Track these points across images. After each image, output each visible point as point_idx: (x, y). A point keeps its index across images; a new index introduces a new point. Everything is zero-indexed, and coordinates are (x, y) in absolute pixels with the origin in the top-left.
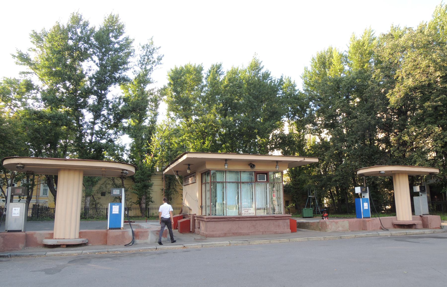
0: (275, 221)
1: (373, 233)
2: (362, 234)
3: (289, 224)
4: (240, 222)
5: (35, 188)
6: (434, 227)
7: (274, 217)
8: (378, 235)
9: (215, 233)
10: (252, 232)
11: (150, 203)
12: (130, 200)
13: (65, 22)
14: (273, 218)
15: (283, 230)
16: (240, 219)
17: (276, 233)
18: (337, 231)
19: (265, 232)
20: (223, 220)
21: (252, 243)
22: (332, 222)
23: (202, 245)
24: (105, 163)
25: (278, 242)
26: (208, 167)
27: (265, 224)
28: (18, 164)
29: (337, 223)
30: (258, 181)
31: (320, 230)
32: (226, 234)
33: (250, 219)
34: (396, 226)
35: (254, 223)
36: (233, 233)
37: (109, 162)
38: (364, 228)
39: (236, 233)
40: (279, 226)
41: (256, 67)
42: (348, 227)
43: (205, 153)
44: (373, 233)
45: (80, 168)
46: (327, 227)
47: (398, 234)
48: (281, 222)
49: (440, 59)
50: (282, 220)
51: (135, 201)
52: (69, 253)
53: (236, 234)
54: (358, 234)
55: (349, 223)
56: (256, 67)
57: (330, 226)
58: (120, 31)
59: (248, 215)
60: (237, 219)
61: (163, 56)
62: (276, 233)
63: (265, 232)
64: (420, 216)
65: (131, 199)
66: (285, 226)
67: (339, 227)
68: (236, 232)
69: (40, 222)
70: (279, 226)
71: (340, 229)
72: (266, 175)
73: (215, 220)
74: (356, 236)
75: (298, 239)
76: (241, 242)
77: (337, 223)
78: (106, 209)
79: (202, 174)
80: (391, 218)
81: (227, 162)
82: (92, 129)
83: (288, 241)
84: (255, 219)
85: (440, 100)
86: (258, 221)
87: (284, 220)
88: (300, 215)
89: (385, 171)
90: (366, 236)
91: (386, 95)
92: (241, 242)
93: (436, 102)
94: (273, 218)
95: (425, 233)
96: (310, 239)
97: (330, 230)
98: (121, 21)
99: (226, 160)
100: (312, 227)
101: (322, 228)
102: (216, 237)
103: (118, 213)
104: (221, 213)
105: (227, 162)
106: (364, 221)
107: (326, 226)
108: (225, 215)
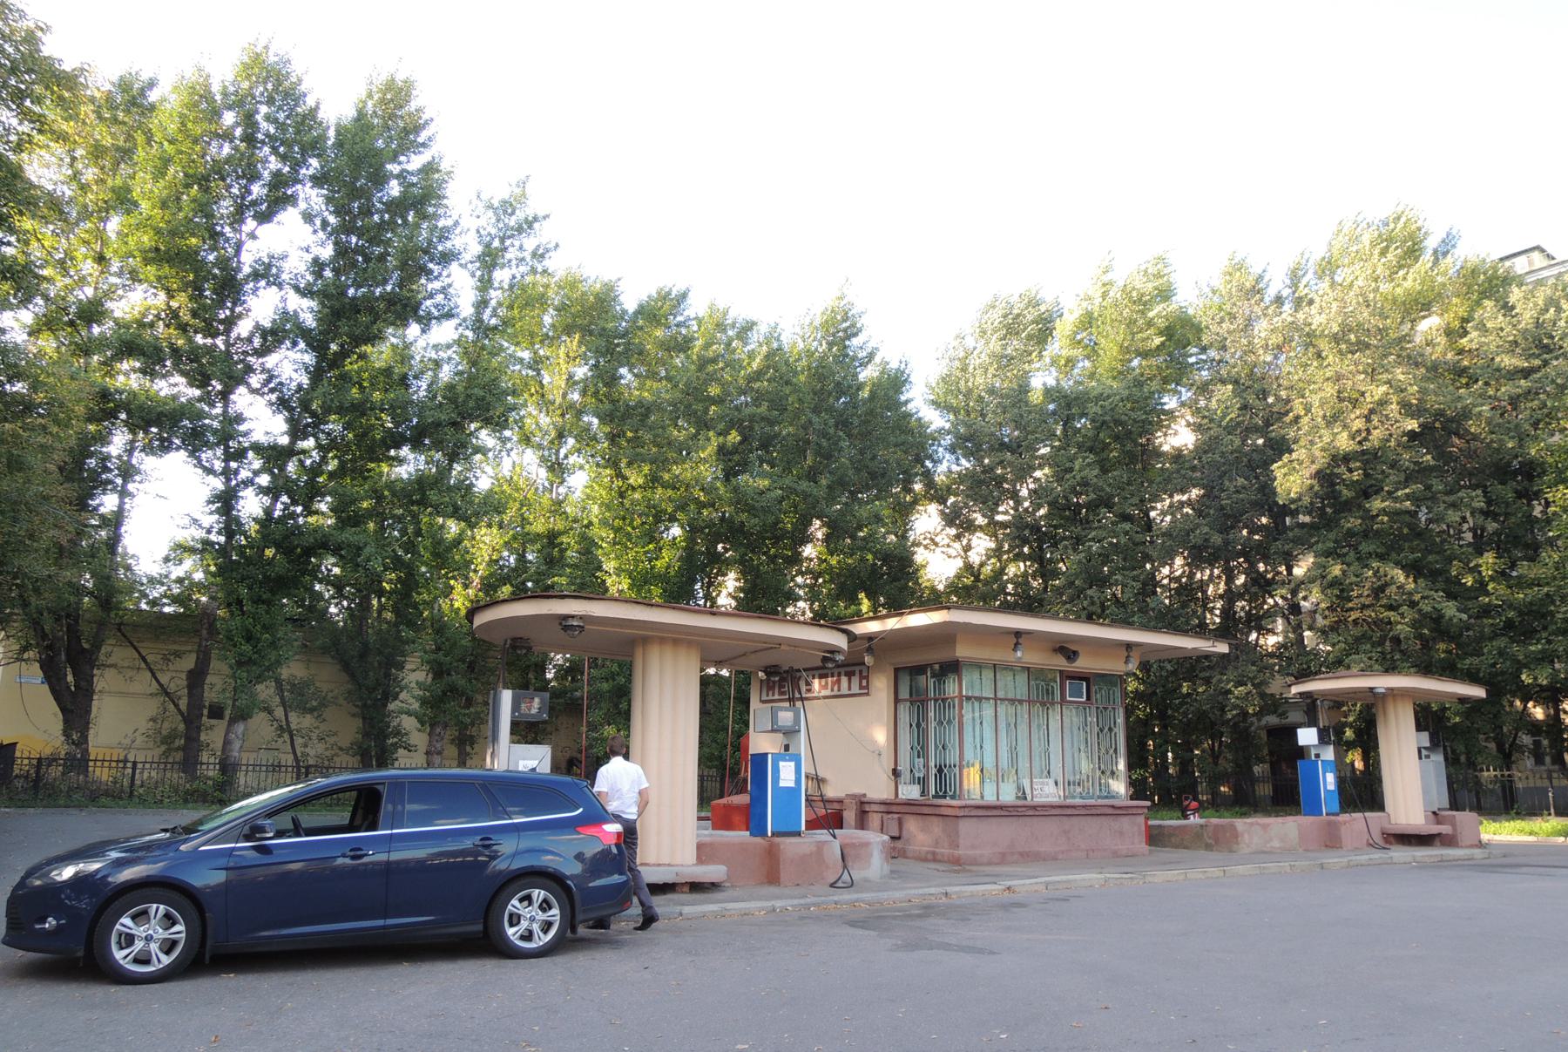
2: (1333, 859)
5: (787, 704)
6: (1469, 843)
7: (1113, 807)
9: (978, 852)
11: (401, 752)
12: (332, 740)
13: (223, 74)
14: (1110, 811)
16: (1023, 810)
17: (1116, 854)
21: (1150, 879)
22: (1252, 824)
23: (1047, 884)
24: (805, 627)
25: (1201, 876)
27: (1092, 825)
28: (573, 617)
29: (1265, 827)
31: (1208, 847)
32: (1003, 855)
34: (1392, 839)
36: (1021, 854)
37: (714, 614)
38: (1331, 840)
40: (1121, 833)
41: (841, 329)
45: (694, 635)
46: (1237, 837)
47: (1427, 859)
48: (1125, 822)
49: (1416, 388)
51: (345, 743)
52: (740, 909)
56: (841, 329)
57: (1246, 836)
58: (409, 134)
60: (1031, 813)
61: (557, 246)
62: (1116, 854)
64: (1434, 813)
65: (335, 734)
66: (1133, 829)
67: (1271, 840)
69: (72, 811)
70: (1121, 833)
71: (1276, 844)
73: (980, 812)
78: (129, 765)
79: (897, 671)
85: (1408, 497)
89: (1388, 689)
91: (1273, 468)
93: (1396, 499)
94: (1110, 811)
98: (423, 100)
99: (1018, 634)
100: (1173, 840)
101: (1220, 842)
103: (792, 784)
106: (1329, 823)
107: (1235, 835)
108: (1029, 798)
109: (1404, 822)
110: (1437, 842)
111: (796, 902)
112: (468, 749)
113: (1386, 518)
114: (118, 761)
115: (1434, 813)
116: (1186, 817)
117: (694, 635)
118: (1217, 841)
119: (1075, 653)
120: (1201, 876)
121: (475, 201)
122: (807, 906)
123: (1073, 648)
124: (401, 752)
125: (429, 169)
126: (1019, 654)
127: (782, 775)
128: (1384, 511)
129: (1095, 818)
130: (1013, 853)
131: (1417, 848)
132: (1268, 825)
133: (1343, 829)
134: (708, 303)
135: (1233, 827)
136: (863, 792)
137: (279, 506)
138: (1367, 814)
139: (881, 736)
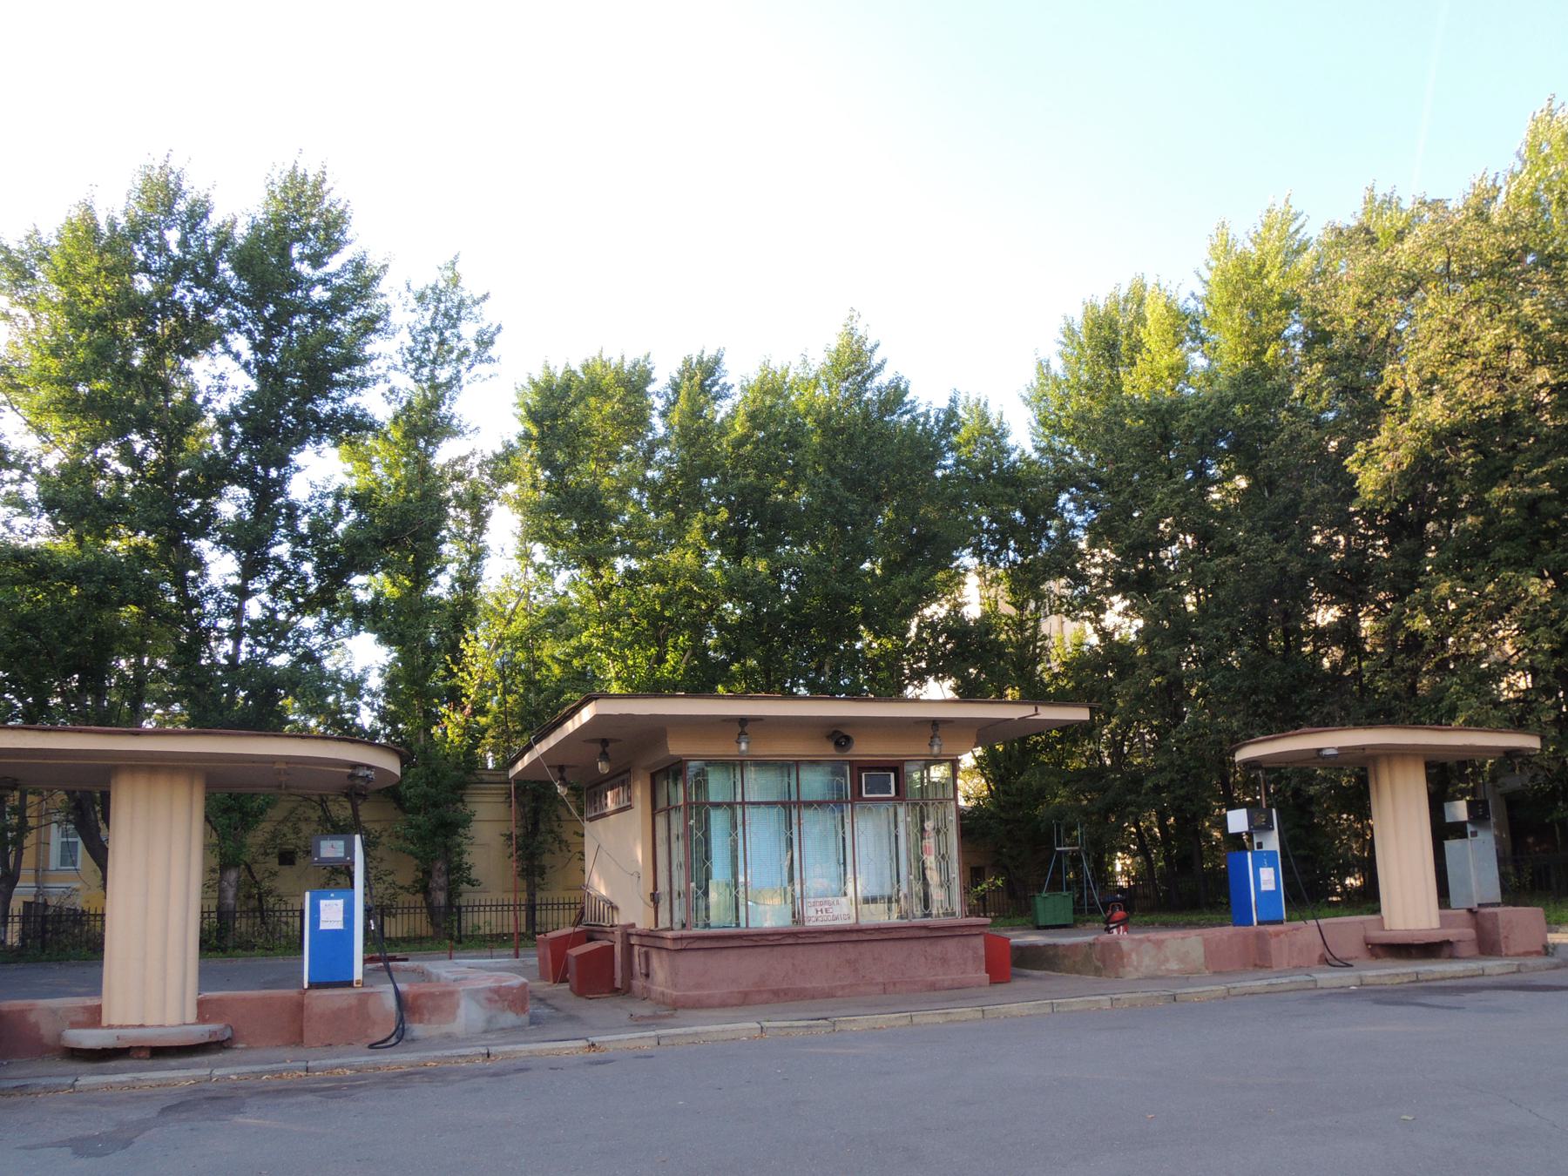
0: (927, 942)
1: (1293, 978)
3: (982, 952)
4: (800, 948)
8: (1311, 986)
10: (843, 988)
11: (464, 886)
12: (389, 879)
14: (923, 933)
17: (933, 987)
18: (1160, 973)
19: (894, 984)
21: (843, 1026)
22: (1141, 941)
23: (659, 1038)
25: (940, 1020)
27: (893, 953)
29: (1159, 944)
30: (864, 795)
31: (1098, 972)
32: (746, 994)
34: (1378, 950)
35: (851, 952)
36: (776, 993)
38: (1260, 960)
39: (786, 992)
40: (944, 961)
42: (1202, 960)
44: (1293, 978)
45: (188, 761)
46: (1122, 958)
47: (1387, 980)
48: (951, 947)
50: (956, 939)
52: (160, 1079)
54: (1238, 985)
55: (1206, 943)
56: (765, 367)
57: (1134, 956)
58: (331, 233)
59: (828, 923)
62: (933, 987)
63: (894, 984)
64: (1470, 910)
65: (392, 873)
67: (1167, 960)
68: (785, 986)
71: (1174, 965)
72: (892, 775)
73: (707, 944)
75: (1015, 1008)
77: (1159, 944)
80: (1362, 923)
82: (237, 613)
83: (979, 1015)
84: (854, 937)
85: (1549, 475)
86: (866, 944)
87: (962, 939)
89: (1339, 749)
90: (1292, 986)
91: (1346, 463)
93: (1533, 483)
94: (923, 933)
95: (1487, 972)
96: (1059, 1005)
97: (1136, 969)
98: (338, 193)
99: (743, 721)
101: (1104, 963)
103: (339, 926)
104: (729, 918)
108: (743, 924)
109: (1402, 927)
110: (1446, 950)
111: (245, 1069)
112: (537, 879)
113: (1511, 510)
114: (415, 908)
115: (1470, 910)
116: (1108, 930)
117: (188, 761)
118: (1104, 962)
119: (848, 739)
120: (940, 1020)
121: (405, 294)
122: (259, 1075)
123: (847, 732)
124: (464, 886)
125: (358, 267)
126: (743, 746)
127: (323, 917)
128: (1505, 501)
129: (899, 944)
130: (760, 992)
131: (1419, 962)
132: (1163, 941)
133: (1273, 941)
134: (542, 363)
135: (1115, 945)
136: (632, 921)
137: (243, 647)
138: (1321, 922)
139: (639, 853)
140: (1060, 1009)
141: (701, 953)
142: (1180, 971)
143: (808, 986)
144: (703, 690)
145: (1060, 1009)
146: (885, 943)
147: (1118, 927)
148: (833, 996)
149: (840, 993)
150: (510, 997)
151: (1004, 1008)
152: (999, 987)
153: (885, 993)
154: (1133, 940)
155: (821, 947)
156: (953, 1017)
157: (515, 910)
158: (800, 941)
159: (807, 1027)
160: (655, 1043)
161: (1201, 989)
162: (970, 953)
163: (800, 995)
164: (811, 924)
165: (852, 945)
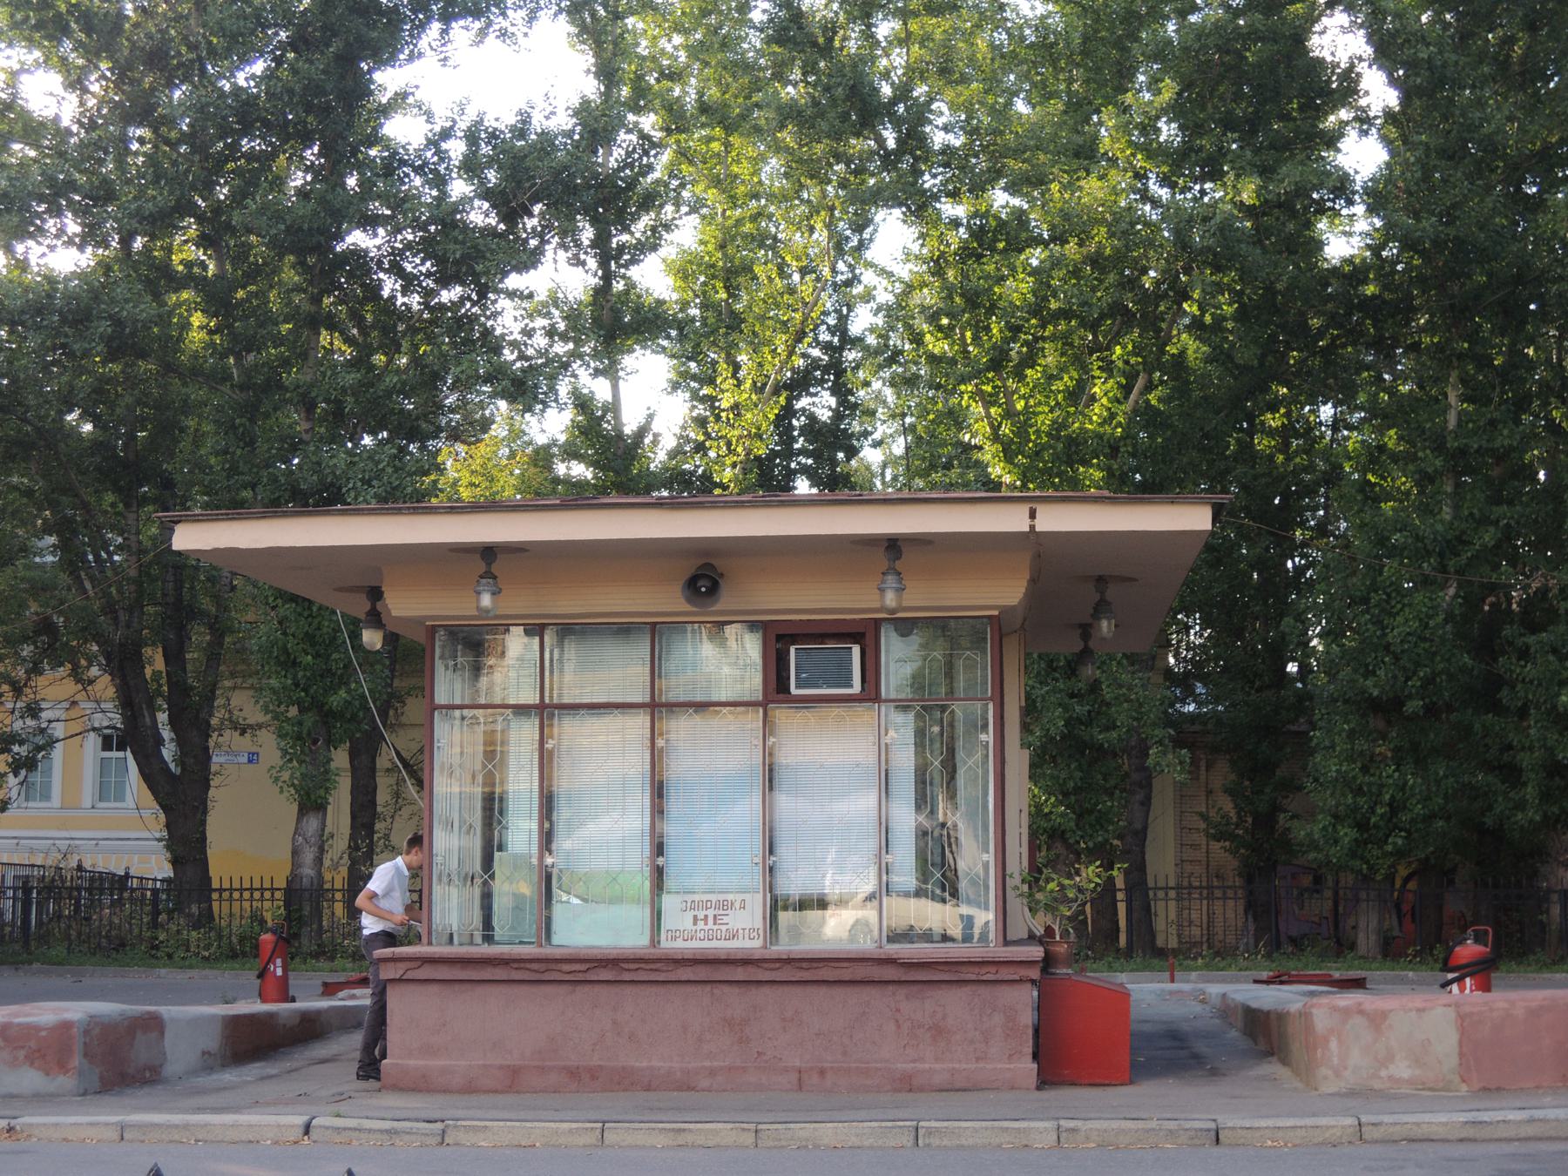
0: (902, 992)
3: (1027, 1018)
4: (629, 990)
10: (712, 1073)
14: (890, 973)
15: (973, 1066)
17: (907, 1085)
18: (1377, 1085)
19: (822, 1072)
20: (500, 973)
21: (462, 1137)
22: (1346, 1013)
23: (122, 1128)
25: (660, 1141)
26: (402, 605)
30: (794, 691)
33: (702, 973)
35: (735, 1002)
36: (573, 1073)
39: (593, 1073)
40: (939, 1032)
42: (1454, 1061)
43: (285, 515)
48: (954, 1004)
50: (967, 989)
53: (594, 1078)
54: (1387, 1119)
55: (1466, 1024)
59: (715, 944)
63: (822, 1072)
67: (1390, 1058)
68: (595, 1061)
71: (1402, 1069)
72: (856, 650)
74: (1368, 1133)
75: (828, 1132)
76: (387, 1125)
77: (1377, 1020)
81: (495, 569)
82: (1417, 192)
83: (749, 1139)
84: (740, 974)
86: (766, 990)
87: (984, 991)
88: (1339, 965)
90: (1530, 1131)
92: (387, 1125)
94: (890, 973)
97: (1337, 1074)
102: (446, 1091)
104: (529, 929)
105: (495, 569)
114: (251, 889)
129: (839, 992)
132: (1384, 1015)
140: (935, 1141)
141: (434, 988)
142: (1410, 1082)
143: (637, 1064)
144: (331, 502)
145: (935, 1141)
146: (810, 990)
147: (1460, 980)
148: (691, 1088)
149: (705, 1083)
150: (33, 1044)
151: (803, 1131)
152: (1051, 1095)
153: (800, 1088)
154: (1335, 1009)
155: (673, 989)
156: (689, 1138)
157: (1179, 899)
158: (627, 977)
159: (388, 1131)
160: (115, 1136)
161: (1290, 1122)
162: (998, 1019)
163: (623, 1081)
164: (679, 944)
165: (735, 990)
